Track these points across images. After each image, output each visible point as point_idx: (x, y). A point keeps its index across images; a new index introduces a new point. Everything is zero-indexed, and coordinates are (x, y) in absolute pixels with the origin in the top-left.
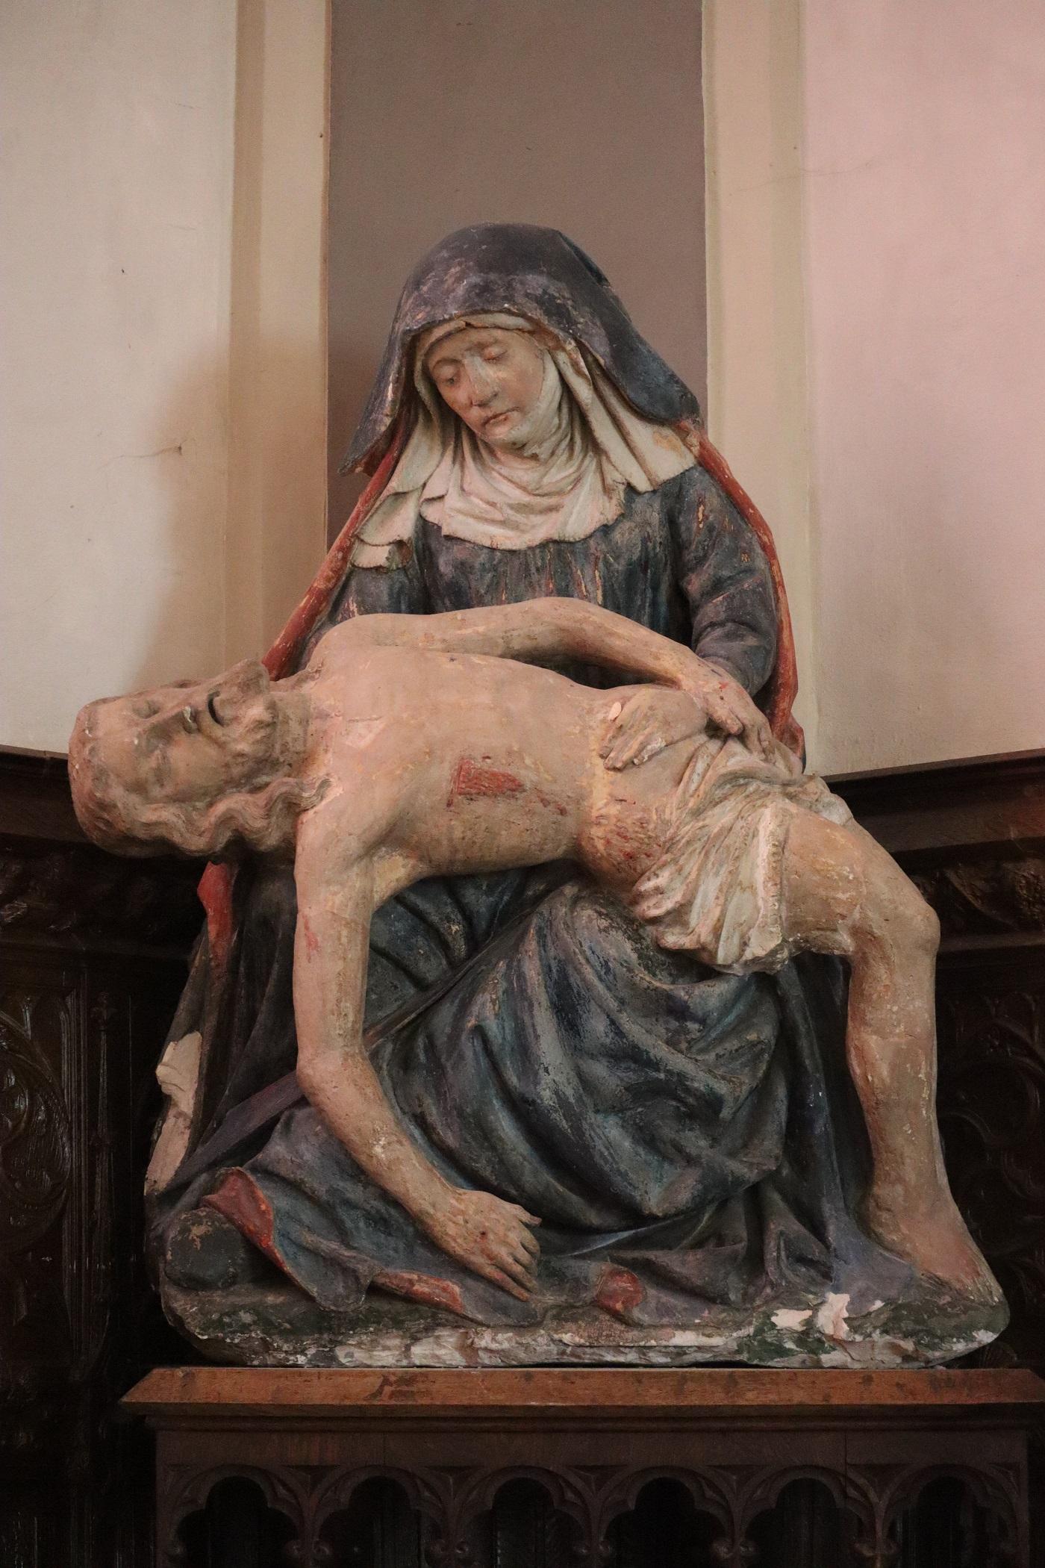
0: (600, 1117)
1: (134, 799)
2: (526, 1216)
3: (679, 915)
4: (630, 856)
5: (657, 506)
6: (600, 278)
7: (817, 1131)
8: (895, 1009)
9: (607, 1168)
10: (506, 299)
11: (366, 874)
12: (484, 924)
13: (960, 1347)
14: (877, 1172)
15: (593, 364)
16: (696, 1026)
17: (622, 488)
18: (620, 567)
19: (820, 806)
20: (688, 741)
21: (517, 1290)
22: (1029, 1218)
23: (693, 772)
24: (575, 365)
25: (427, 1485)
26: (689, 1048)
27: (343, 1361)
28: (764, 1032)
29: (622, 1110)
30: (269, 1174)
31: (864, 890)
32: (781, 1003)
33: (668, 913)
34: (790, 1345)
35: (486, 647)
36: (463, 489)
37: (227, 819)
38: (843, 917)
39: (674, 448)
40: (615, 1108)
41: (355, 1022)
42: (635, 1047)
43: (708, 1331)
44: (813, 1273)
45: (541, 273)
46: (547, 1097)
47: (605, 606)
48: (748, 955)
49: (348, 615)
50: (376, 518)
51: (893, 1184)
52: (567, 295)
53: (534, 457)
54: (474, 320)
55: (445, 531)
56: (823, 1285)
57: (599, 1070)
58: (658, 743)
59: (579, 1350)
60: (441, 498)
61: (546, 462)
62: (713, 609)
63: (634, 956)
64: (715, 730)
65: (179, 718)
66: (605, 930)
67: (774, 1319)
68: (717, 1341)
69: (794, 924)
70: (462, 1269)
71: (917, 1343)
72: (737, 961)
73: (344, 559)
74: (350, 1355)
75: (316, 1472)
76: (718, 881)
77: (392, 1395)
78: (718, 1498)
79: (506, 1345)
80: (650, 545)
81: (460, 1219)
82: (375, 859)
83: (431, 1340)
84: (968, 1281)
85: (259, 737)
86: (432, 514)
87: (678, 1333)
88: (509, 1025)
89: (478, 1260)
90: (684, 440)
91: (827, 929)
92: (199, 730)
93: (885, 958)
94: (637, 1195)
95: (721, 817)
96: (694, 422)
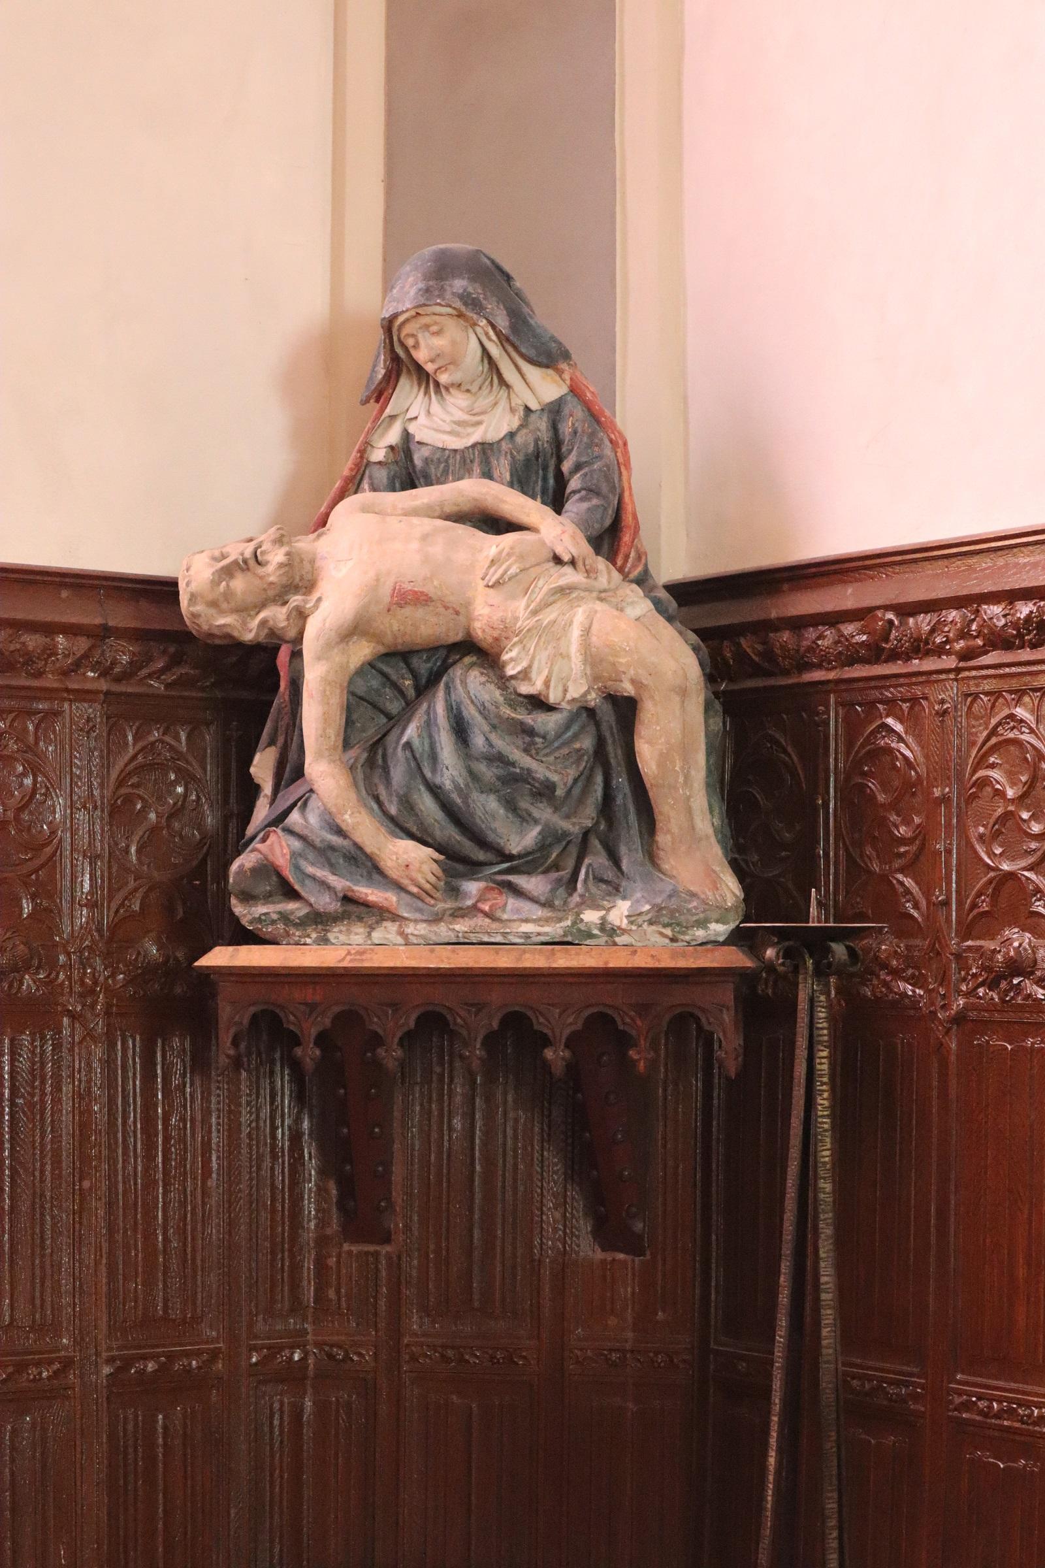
0: (484, 796)
1: (212, 611)
2: (436, 855)
3: (525, 675)
4: (497, 639)
5: (545, 418)
6: (508, 278)
7: (618, 803)
8: (658, 728)
9: (483, 826)
10: (439, 296)
11: (343, 654)
12: (424, 681)
13: (700, 934)
14: (657, 827)
15: (498, 334)
16: (541, 740)
17: (521, 409)
18: (520, 457)
19: (624, 604)
20: (537, 567)
21: (428, 899)
22: (783, 854)
23: (535, 587)
24: (487, 334)
25: (292, 1013)
26: (537, 753)
27: (333, 941)
28: (587, 743)
29: (498, 791)
30: (290, 831)
31: (636, 657)
32: (597, 725)
33: (519, 673)
34: (596, 932)
35: (427, 512)
36: (429, 412)
37: (264, 623)
38: (624, 673)
39: (555, 382)
40: (491, 790)
41: (336, 741)
42: (500, 753)
43: (541, 923)
44: (610, 888)
45: (463, 279)
46: (448, 785)
47: (511, 485)
48: (569, 697)
49: (364, 491)
50: (379, 431)
51: (666, 834)
52: (480, 291)
53: (468, 391)
54: (420, 311)
55: (417, 439)
56: (615, 895)
57: (482, 768)
58: (514, 570)
59: (466, 935)
60: (416, 418)
61: (476, 393)
62: (574, 483)
63: (501, 699)
64: (557, 560)
65: (236, 562)
66: (483, 684)
67: (582, 916)
68: (547, 929)
69: (596, 678)
70: (400, 887)
71: (673, 931)
72: (563, 700)
73: (362, 457)
74: (337, 938)
75: (312, 1007)
76: (547, 653)
77: (351, 961)
78: (546, 1023)
79: (422, 932)
80: (540, 443)
81: (394, 857)
82: (351, 643)
83: (382, 928)
84: (710, 894)
85: (281, 572)
86: (412, 428)
87: (524, 925)
88: (426, 742)
89: (405, 882)
90: (560, 376)
91: (616, 681)
92: (248, 569)
93: (652, 697)
94: (502, 842)
95: (548, 616)
96: (569, 365)
